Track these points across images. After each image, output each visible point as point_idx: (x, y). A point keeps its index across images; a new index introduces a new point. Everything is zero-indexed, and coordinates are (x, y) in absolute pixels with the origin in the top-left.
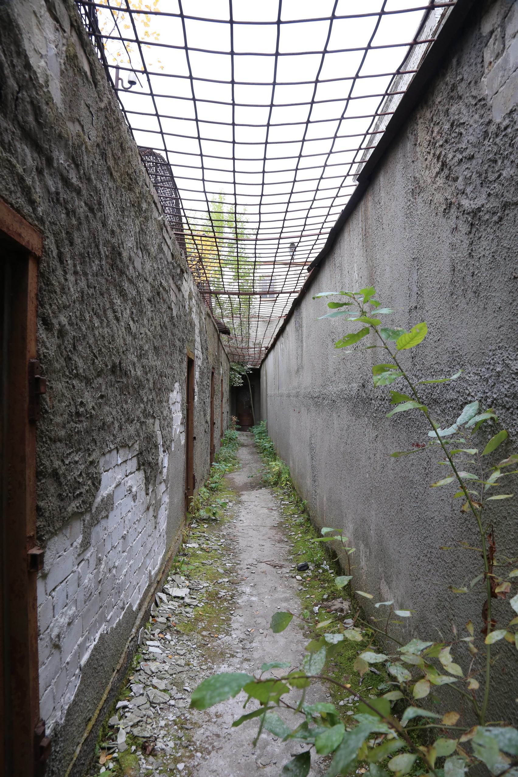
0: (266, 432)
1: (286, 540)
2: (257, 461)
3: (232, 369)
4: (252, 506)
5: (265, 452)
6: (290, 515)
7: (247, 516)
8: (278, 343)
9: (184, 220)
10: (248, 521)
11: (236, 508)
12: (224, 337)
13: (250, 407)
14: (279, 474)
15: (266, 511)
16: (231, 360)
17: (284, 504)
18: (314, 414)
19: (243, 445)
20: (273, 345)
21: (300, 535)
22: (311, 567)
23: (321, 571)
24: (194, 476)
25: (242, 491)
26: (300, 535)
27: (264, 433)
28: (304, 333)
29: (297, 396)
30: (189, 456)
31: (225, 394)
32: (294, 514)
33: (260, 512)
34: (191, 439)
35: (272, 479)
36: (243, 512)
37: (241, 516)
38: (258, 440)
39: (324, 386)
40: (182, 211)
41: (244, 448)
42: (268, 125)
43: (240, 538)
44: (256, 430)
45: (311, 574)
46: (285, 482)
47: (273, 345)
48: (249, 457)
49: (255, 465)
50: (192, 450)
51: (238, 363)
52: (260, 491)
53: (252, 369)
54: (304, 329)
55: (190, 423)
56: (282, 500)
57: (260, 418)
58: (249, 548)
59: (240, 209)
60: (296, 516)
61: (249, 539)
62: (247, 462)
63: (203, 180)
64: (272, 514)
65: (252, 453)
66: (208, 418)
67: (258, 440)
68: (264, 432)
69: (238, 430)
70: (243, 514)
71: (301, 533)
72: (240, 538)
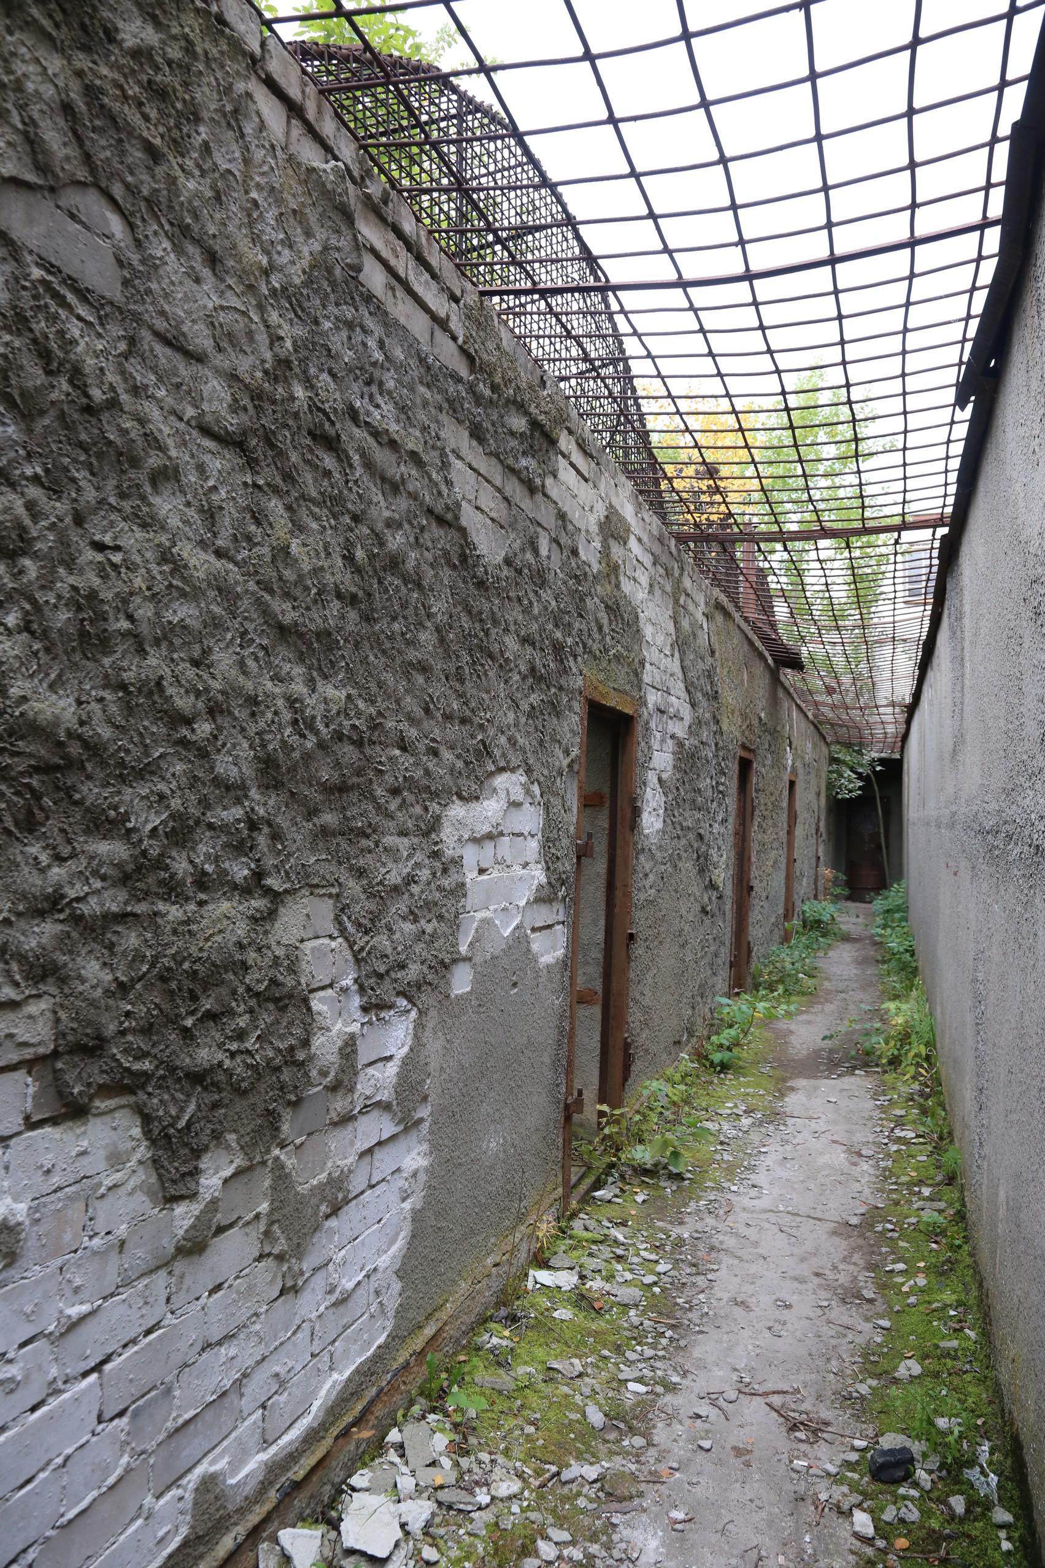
0: (903, 909)
1: (868, 1294)
2: (866, 986)
3: (834, 760)
4: (806, 1135)
5: (893, 963)
6: (910, 1184)
7: (780, 1172)
8: (926, 688)
9: (632, 346)
10: (776, 1191)
11: (755, 1137)
12: (789, 676)
13: (879, 847)
14: (905, 1037)
15: (839, 1157)
16: (829, 739)
17: (899, 1140)
18: (985, 886)
19: (846, 938)
20: (917, 696)
21: (921, 1281)
22: (921, 1475)
23: (958, 1503)
24: (627, 1046)
25: (800, 1075)
26: (921, 1281)
27: (900, 913)
28: (968, 635)
29: (951, 826)
30: (614, 986)
31: (803, 815)
32: (921, 1183)
33: (822, 1160)
34: (619, 940)
35: (885, 1048)
36: (773, 1153)
37: (762, 1170)
38: (879, 931)
39: (1010, 792)
40: (619, 319)
41: (847, 946)
42: (912, 165)
43: (727, 1260)
44: (879, 904)
45: (913, 1515)
46: (912, 1069)
47: (917, 696)
48: (852, 971)
49: (859, 996)
50: (625, 971)
51: (848, 745)
52: (848, 1082)
53: (882, 761)
54: (967, 621)
55: (619, 893)
56: (900, 1122)
57: (899, 874)
58: (738, 1312)
59: (856, 393)
60: (926, 1192)
61: (753, 1269)
62: (841, 986)
63: (762, 328)
64: (856, 1171)
65: (862, 962)
66: (723, 875)
67: (879, 931)
68: (899, 909)
69: (837, 898)
70: (769, 1161)
71: (926, 1270)
72: (727, 1260)
